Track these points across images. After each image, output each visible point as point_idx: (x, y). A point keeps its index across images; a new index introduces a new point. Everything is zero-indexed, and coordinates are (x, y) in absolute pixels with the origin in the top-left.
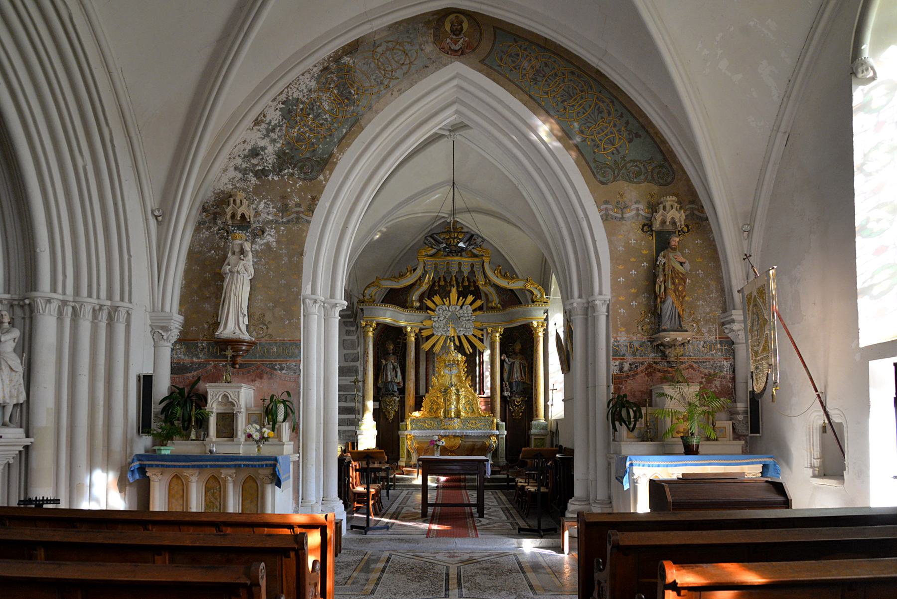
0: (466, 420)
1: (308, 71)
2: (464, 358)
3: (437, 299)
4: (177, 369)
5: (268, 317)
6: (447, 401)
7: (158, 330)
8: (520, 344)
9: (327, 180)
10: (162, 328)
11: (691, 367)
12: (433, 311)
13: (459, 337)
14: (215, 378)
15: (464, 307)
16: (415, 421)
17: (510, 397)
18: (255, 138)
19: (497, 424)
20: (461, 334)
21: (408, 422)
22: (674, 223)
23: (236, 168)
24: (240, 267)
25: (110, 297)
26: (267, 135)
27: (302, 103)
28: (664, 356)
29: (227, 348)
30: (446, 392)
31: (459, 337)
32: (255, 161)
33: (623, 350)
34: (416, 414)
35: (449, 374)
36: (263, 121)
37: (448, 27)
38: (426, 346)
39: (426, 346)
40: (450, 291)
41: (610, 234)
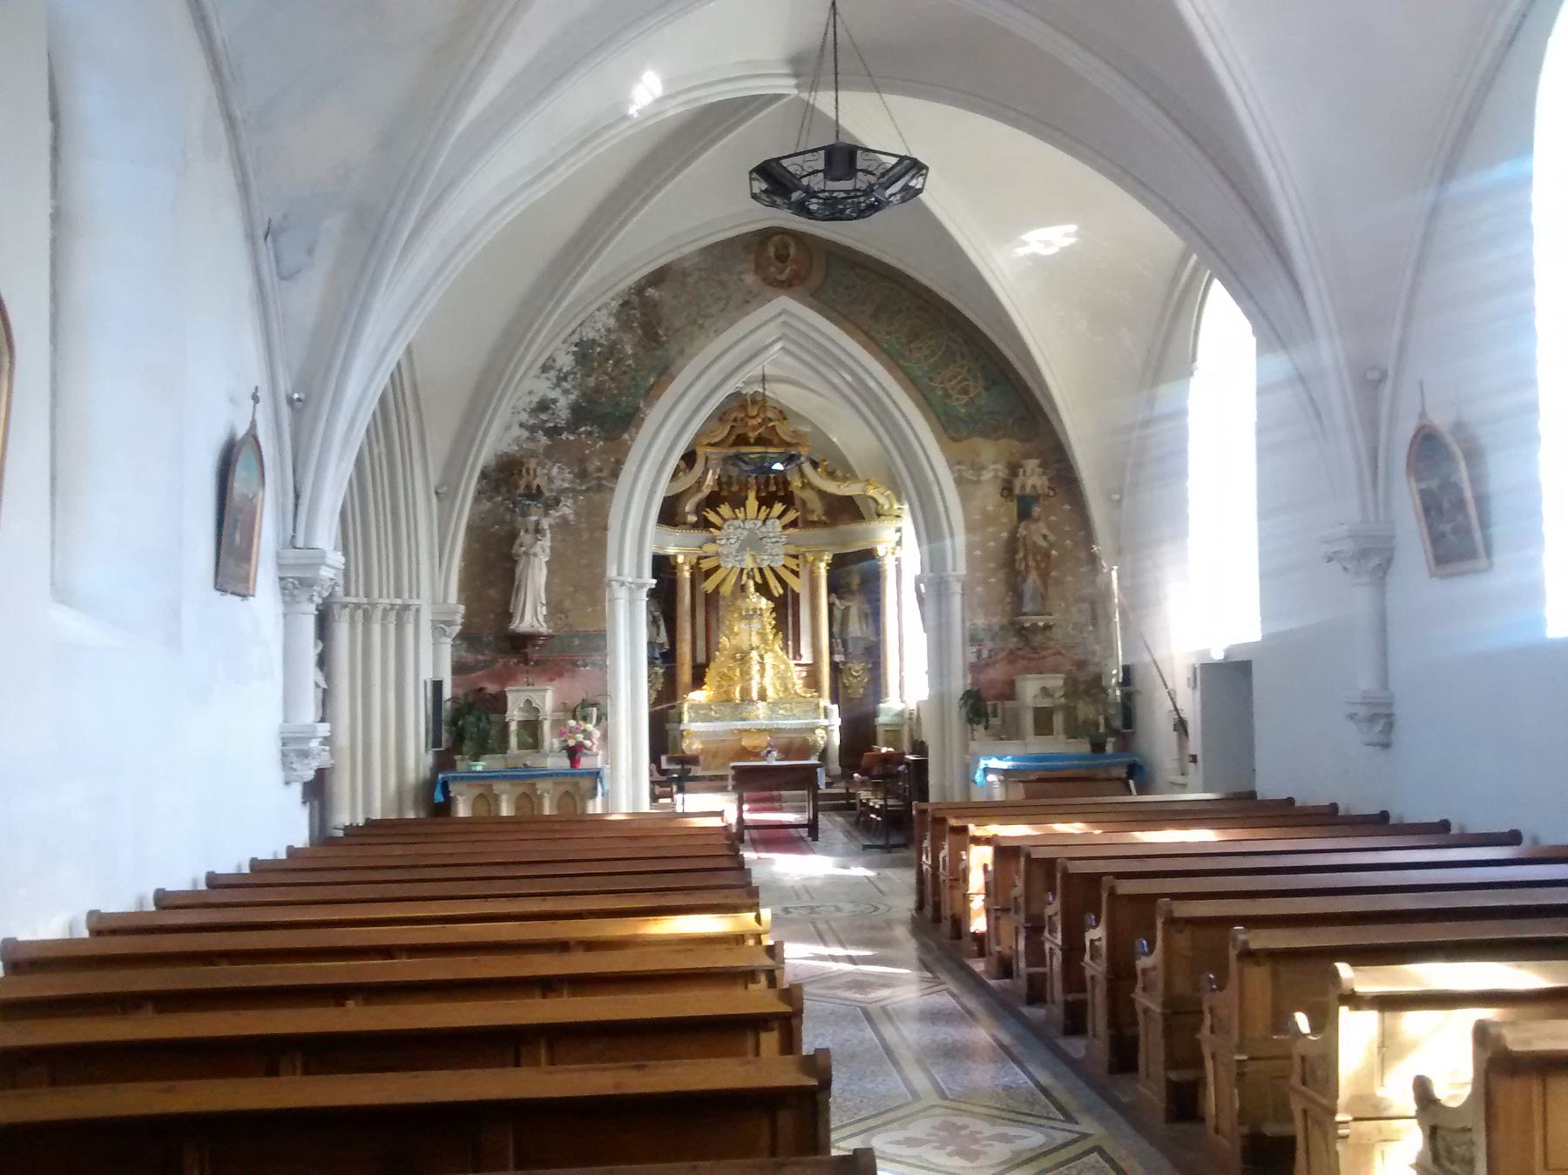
0: (775, 704)
1: (606, 305)
2: (771, 605)
3: (725, 510)
4: (459, 669)
5: (567, 604)
6: (745, 674)
7: (439, 628)
8: (856, 578)
9: (633, 440)
10: (444, 622)
11: (1059, 653)
12: (719, 528)
13: (761, 570)
14: (507, 677)
15: (769, 523)
16: (696, 708)
17: (844, 663)
18: (543, 387)
19: (825, 709)
20: (764, 565)
21: (686, 706)
22: (1034, 487)
23: (521, 425)
24: (537, 549)
25: (398, 595)
26: (557, 385)
27: (601, 345)
28: (1027, 641)
29: (520, 644)
30: (742, 658)
31: (761, 570)
32: (544, 417)
33: (981, 635)
34: (699, 696)
35: (749, 627)
36: (552, 368)
37: (771, 251)
38: (709, 585)
39: (709, 585)
40: (746, 498)
41: (965, 498)
